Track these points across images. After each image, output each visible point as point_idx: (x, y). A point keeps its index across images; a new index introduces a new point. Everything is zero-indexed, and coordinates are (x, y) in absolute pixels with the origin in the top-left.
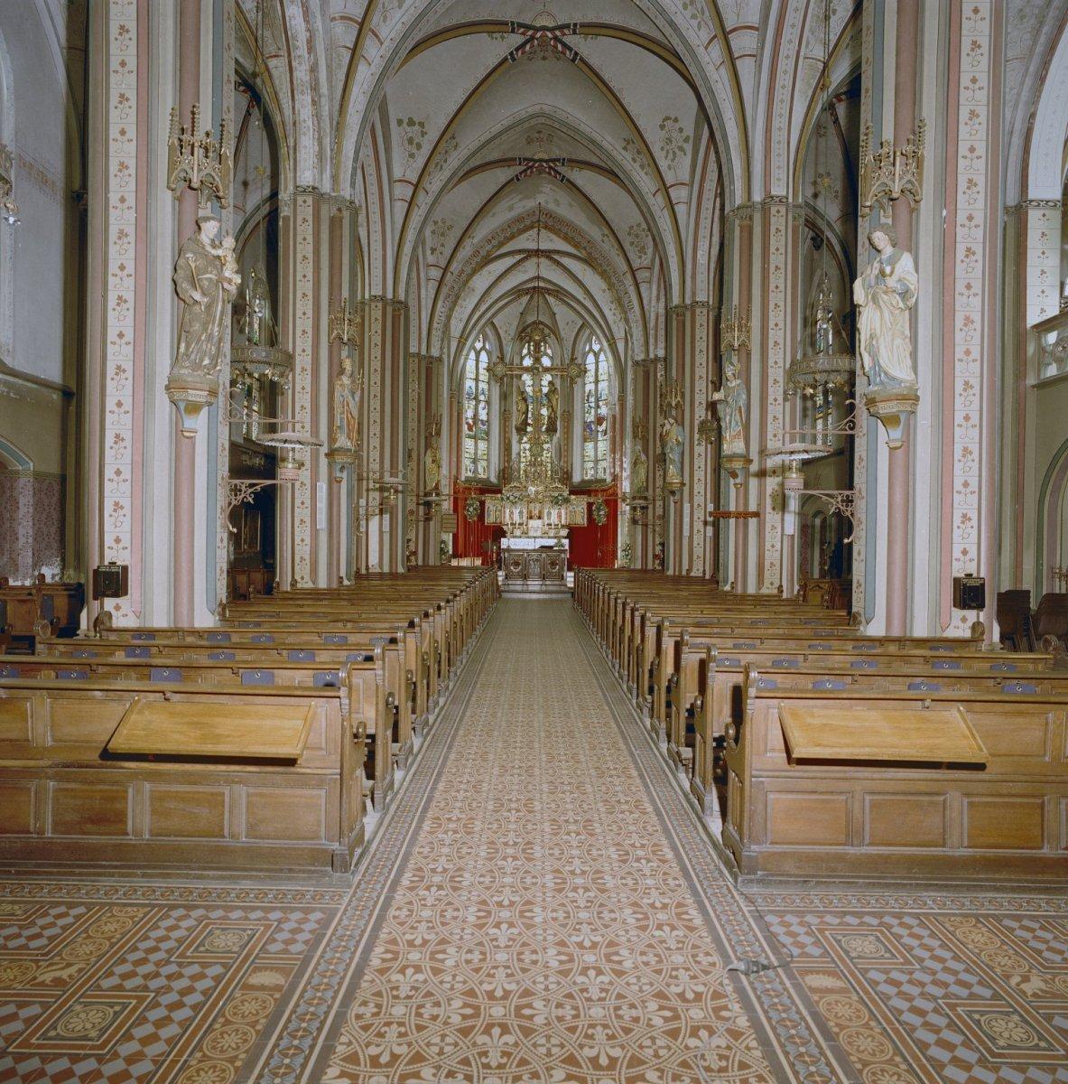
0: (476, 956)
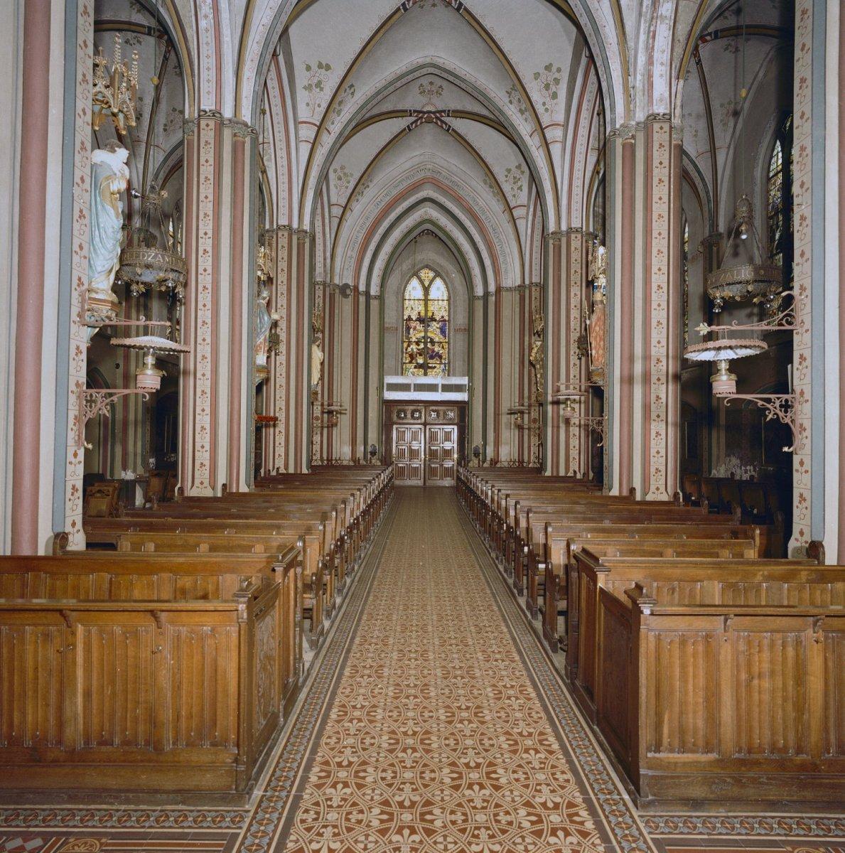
0: (389, 775)
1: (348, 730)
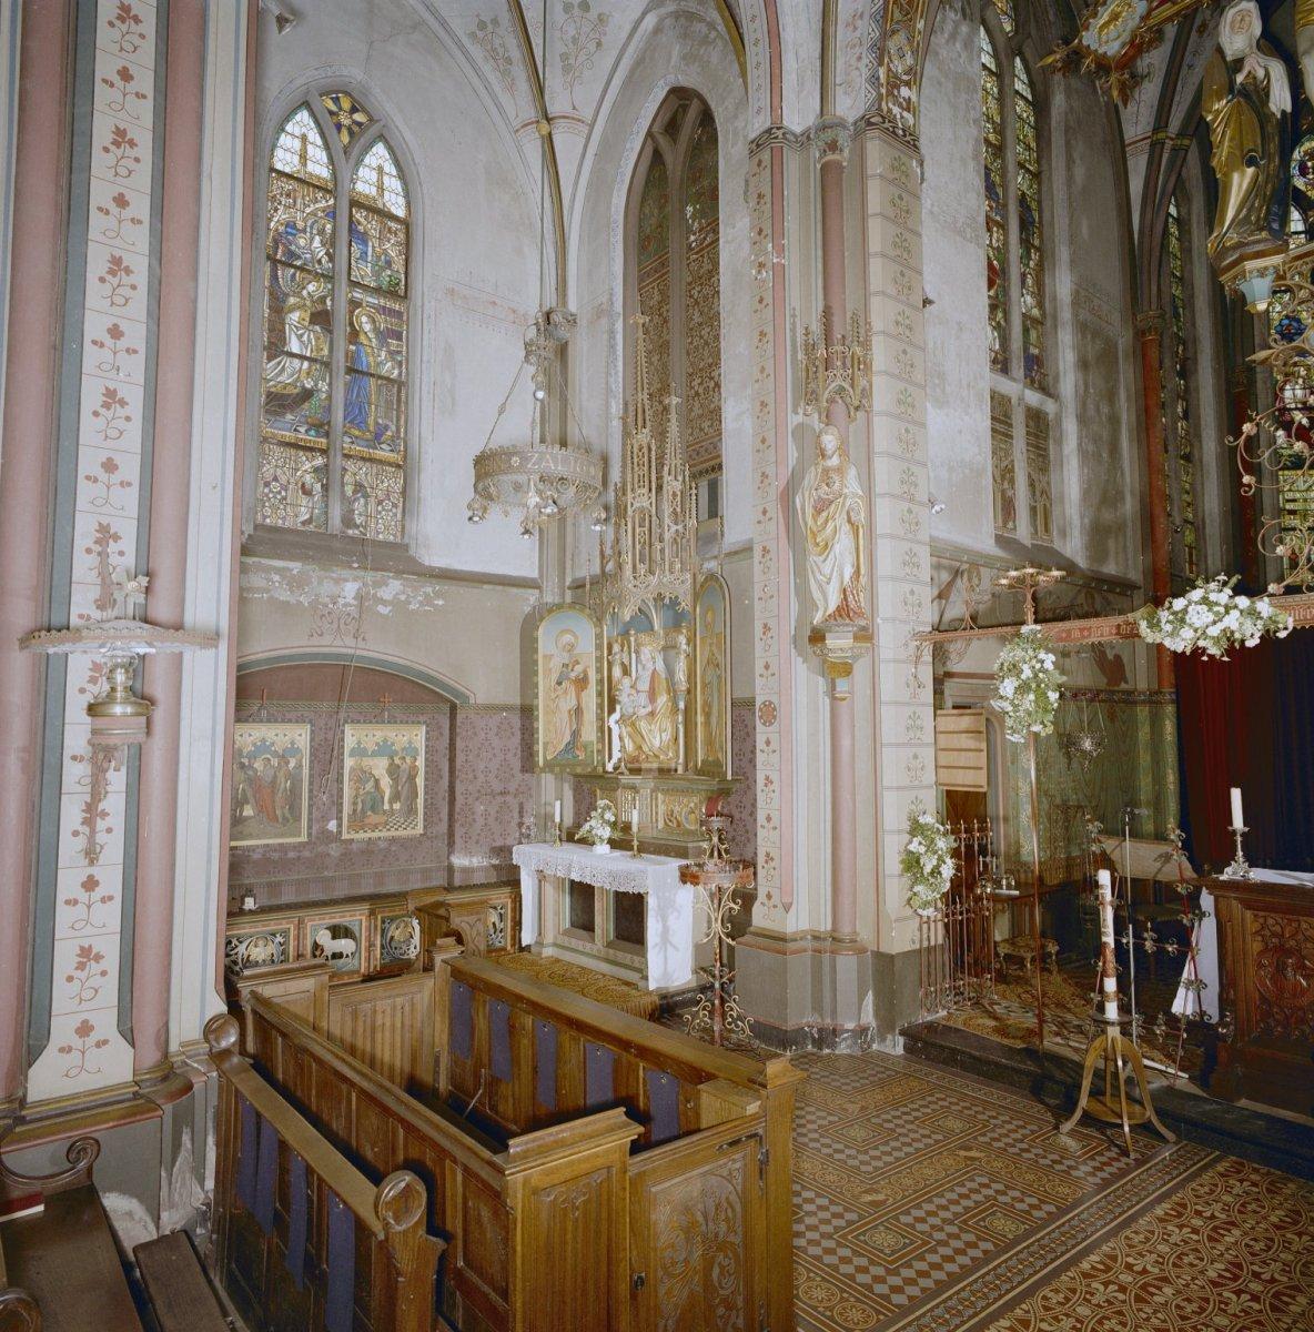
1: (1169, 1235)
